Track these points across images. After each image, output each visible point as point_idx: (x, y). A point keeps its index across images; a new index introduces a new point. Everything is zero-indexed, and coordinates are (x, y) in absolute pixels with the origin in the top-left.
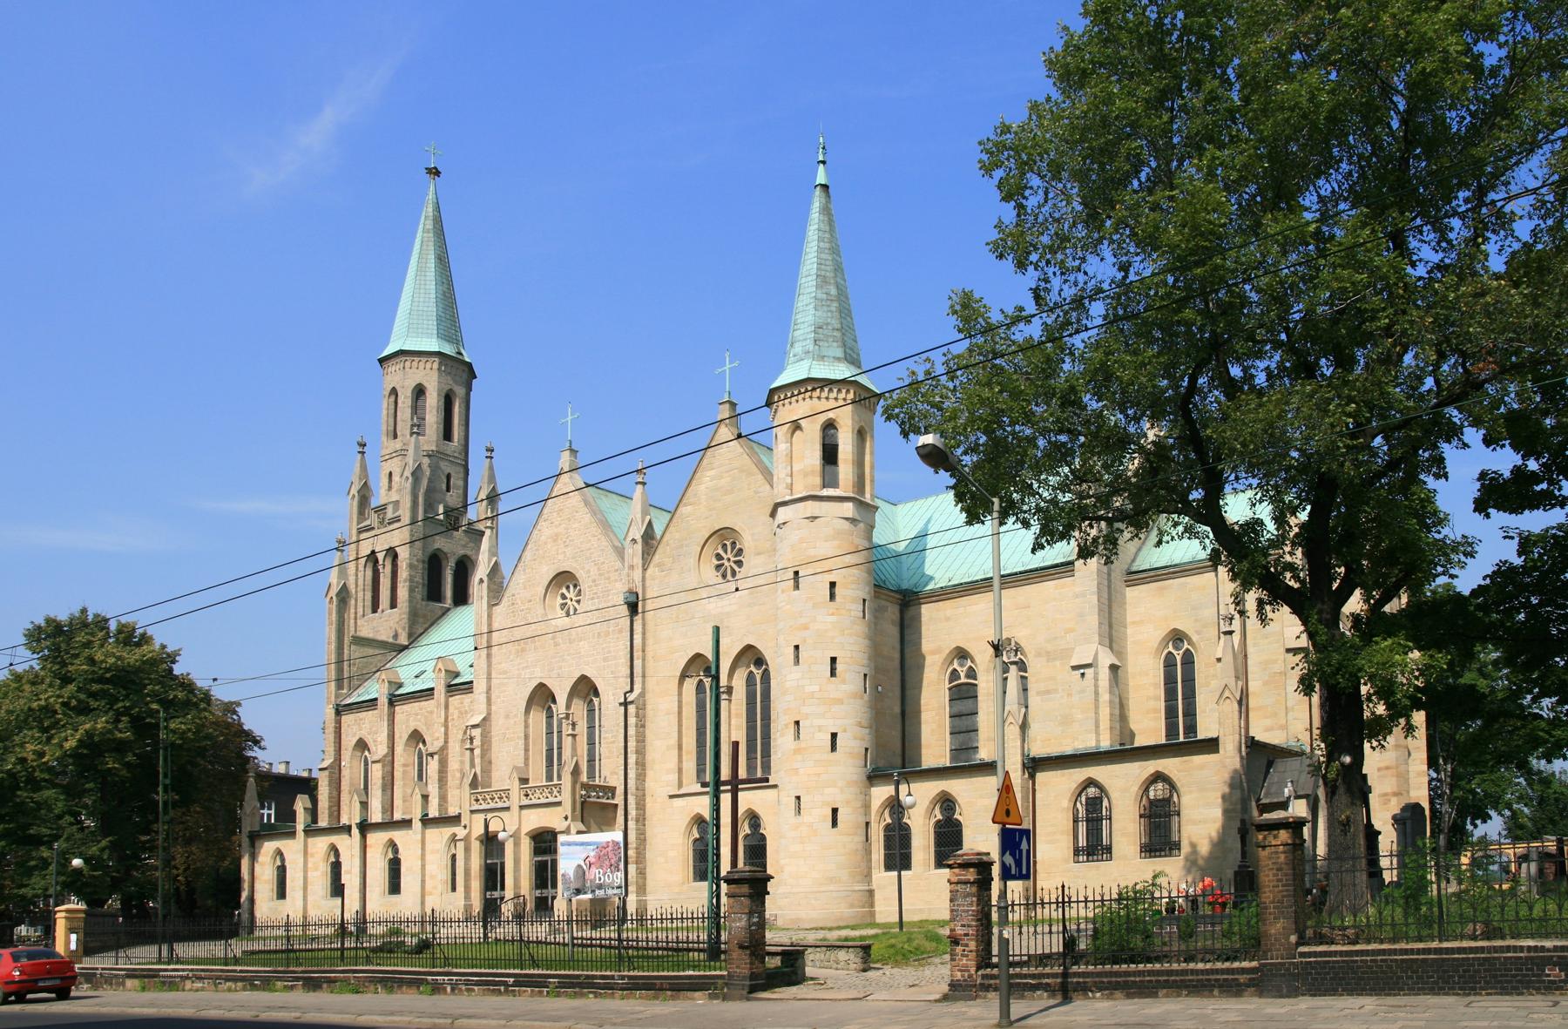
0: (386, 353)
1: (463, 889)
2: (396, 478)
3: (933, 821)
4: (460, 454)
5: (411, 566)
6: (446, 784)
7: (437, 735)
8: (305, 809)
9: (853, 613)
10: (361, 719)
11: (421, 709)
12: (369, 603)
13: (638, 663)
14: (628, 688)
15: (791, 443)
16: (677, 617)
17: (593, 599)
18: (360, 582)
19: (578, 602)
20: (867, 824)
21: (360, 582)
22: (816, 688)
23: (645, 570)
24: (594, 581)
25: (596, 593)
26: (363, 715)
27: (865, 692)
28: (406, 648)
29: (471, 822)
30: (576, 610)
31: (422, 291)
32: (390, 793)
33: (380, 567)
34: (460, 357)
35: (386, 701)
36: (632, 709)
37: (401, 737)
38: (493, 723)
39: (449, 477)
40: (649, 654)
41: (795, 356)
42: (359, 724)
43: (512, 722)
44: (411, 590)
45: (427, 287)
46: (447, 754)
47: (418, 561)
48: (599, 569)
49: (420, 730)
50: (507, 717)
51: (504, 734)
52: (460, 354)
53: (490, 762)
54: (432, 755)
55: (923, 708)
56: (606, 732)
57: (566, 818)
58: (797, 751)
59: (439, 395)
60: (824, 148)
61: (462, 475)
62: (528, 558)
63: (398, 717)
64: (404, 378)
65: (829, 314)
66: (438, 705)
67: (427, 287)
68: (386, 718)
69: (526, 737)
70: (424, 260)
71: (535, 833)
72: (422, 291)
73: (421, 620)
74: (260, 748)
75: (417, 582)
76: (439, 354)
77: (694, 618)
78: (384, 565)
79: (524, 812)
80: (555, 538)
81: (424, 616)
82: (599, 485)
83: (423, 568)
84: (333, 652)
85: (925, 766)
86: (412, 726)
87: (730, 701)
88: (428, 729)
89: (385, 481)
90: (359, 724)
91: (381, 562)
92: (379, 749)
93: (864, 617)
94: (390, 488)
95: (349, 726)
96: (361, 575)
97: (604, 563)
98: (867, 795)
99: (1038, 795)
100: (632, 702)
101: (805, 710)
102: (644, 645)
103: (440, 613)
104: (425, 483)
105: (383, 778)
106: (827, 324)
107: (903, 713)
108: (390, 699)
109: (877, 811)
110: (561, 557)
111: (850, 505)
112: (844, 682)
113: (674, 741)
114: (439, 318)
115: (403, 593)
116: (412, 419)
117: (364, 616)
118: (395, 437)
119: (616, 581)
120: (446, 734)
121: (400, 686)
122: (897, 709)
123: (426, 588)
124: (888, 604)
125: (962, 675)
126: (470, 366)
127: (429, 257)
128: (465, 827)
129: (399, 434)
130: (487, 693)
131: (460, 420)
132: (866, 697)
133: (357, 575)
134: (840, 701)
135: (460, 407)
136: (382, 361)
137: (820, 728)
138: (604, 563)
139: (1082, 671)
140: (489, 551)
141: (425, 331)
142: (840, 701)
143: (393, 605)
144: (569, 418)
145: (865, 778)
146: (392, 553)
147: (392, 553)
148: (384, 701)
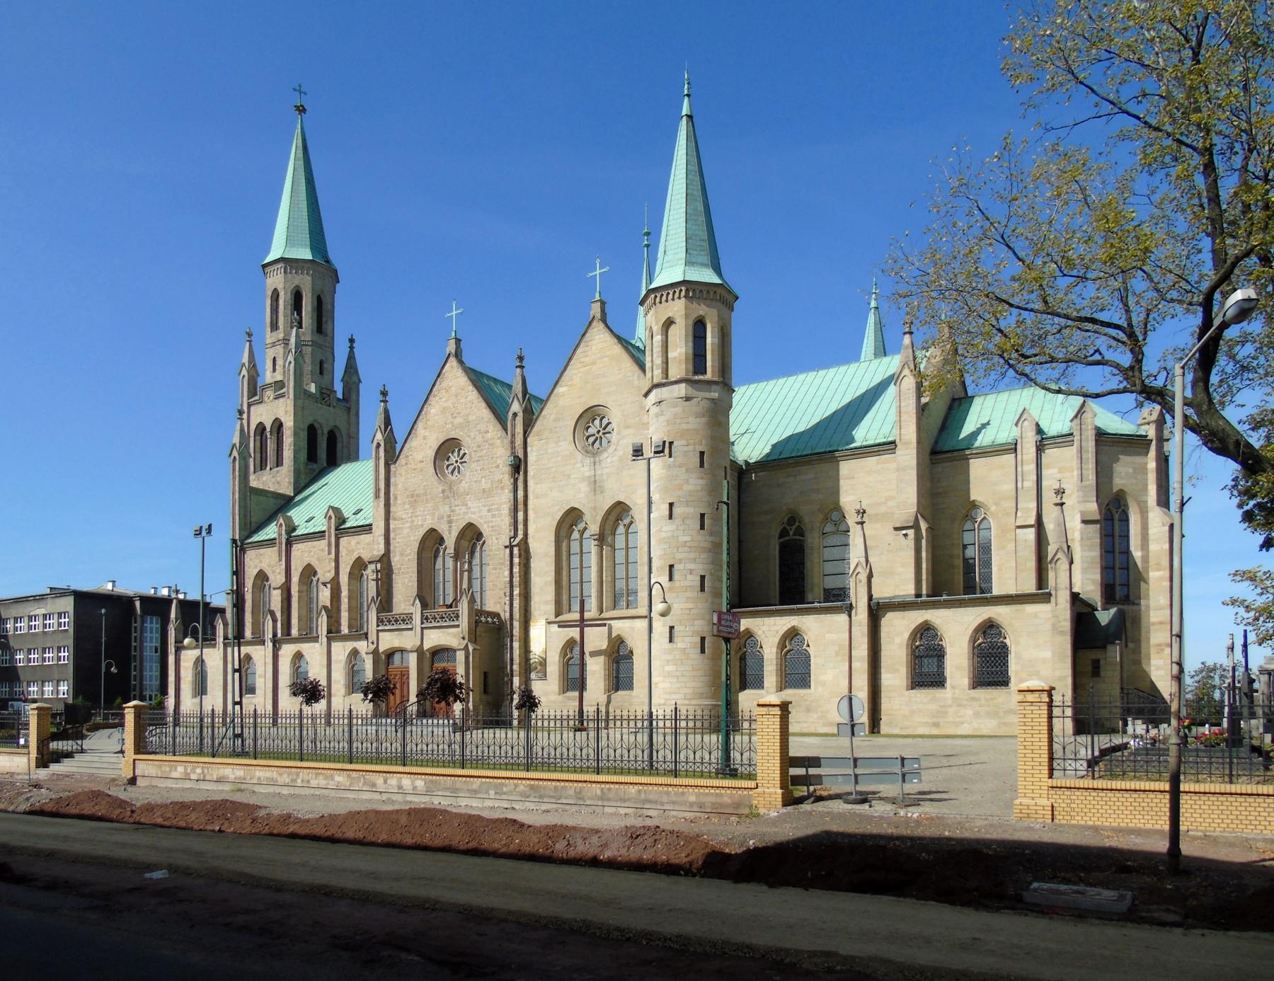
0: (268, 260)
2: (280, 362)
5: (296, 434)
10: (261, 555)
14: (512, 534)
17: (478, 461)
37: (296, 569)
43: (407, 559)
49: (312, 563)
60: (688, 83)
64: (276, 280)
65: (697, 227)
71: (434, 650)
85: (996, 592)
89: (269, 364)
92: (277, 578)
94: (274, 370)
102: (526, 497)
106: (696, 235)
111: (683, 385)
115: (288, 453)
125: (791, 533)
136: (264, 266)
139: (904, 532)
143: (279, 463)
144: (454, 313)
146: (278, 426)
147: (278, 426)
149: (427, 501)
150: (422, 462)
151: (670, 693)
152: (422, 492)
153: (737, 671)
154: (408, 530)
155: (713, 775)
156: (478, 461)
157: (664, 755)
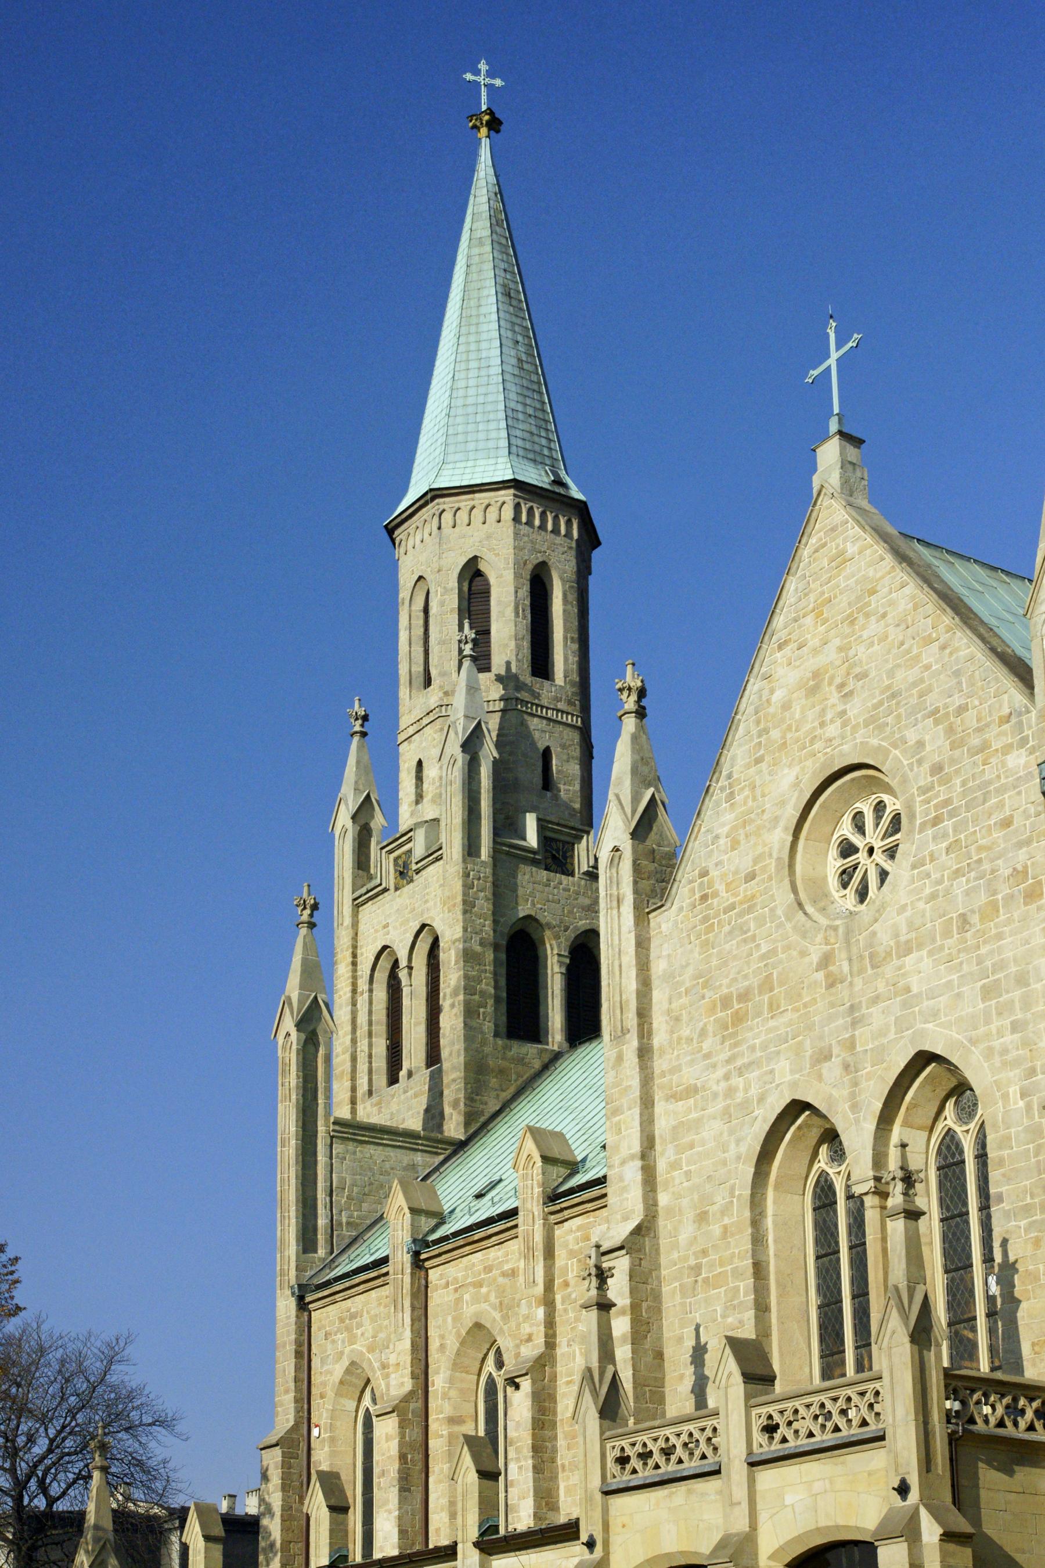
2: (431, 772)
4: (570, 703)
5: (468, 956)
6: (553, 1460)
7: (526, 1329)
8: (207, 1538)
10: (353, 1316)
11: (488, 1269)
12: (381, 1063)
17: (936, 821)
18: (362, 1019)
19: (891, 853)
21: (362, 1019)
24: (937, 769)
25: (947, 802)
26: (357, 1303)
28: (460, 1146)
29: (606, 1527)
30: (883, 875)
31: (473, 364)
32: (419, 1497)
33: (403, 975)
34: (562, 491)
35: (407, 1258)
38: (664, 1242)
39: (547, 754)
42: (348, 1329)
43: (716, 1229)
44: (470, 1012)
46: (554, 1378)
47: (482, 944)
48: (950, 730)
50: (702, 1218)
51: (697, 1269)
52: (558, 482)
53: (660, 1355)
54: (513, 1383)
56: (1007, 1215)
57: (903, 1490)
59: (517, 576)
61: (576, 752)
63: (437, 1299)
66: (528, 1253)
67: (484, 354)
68: (407, 1303)
69: (759, 1270)
70: (473, 303)
72: (473, 364)
73: (494, 1082)
74: (178, 1436)
75: (482, 993)
76: (516, 484)
78: (410, 968)
79: (767, 1477)
80: (813, 686)
81: (502, 1072)
83: (496, 960)
84: (293, 1161)
86: (470, 1312)
88: (506, 1318)
90: (348, 1329)
91: (403, 963)
94: (419, 798)
95: (327, 1336)
96: (362, 1001)
97: (962, 709)
103: (537, 1065)
104: (489, 752)
105: (403, 1457)
108: (417, 1254)
110: (832, 730)
114: (511, 417)
116: (461, 628)
117: (370, 1093)
118: (428, 682)
119: (1007, 749)
120: (550, 1323)
121: (441, 1220)
123: (503, 1008)
126: (581, 510)
127: (485, 292)
128: (590, 1545)
129: (434, 672)
130: (643, 1156)
131: (566, 630)
133: (354, 1004)
138: (962, 709)
140: (635, 771)
141: (481, 445)
148: (402, 1260)
149: (773, 1006)
150: (751, 877)
151: (693, 1053)
152: (755, 981)
153: (590, 1205)
154: (717, 1125)
155: (658, 887)
156: (936, 821)
157: (472, 596)
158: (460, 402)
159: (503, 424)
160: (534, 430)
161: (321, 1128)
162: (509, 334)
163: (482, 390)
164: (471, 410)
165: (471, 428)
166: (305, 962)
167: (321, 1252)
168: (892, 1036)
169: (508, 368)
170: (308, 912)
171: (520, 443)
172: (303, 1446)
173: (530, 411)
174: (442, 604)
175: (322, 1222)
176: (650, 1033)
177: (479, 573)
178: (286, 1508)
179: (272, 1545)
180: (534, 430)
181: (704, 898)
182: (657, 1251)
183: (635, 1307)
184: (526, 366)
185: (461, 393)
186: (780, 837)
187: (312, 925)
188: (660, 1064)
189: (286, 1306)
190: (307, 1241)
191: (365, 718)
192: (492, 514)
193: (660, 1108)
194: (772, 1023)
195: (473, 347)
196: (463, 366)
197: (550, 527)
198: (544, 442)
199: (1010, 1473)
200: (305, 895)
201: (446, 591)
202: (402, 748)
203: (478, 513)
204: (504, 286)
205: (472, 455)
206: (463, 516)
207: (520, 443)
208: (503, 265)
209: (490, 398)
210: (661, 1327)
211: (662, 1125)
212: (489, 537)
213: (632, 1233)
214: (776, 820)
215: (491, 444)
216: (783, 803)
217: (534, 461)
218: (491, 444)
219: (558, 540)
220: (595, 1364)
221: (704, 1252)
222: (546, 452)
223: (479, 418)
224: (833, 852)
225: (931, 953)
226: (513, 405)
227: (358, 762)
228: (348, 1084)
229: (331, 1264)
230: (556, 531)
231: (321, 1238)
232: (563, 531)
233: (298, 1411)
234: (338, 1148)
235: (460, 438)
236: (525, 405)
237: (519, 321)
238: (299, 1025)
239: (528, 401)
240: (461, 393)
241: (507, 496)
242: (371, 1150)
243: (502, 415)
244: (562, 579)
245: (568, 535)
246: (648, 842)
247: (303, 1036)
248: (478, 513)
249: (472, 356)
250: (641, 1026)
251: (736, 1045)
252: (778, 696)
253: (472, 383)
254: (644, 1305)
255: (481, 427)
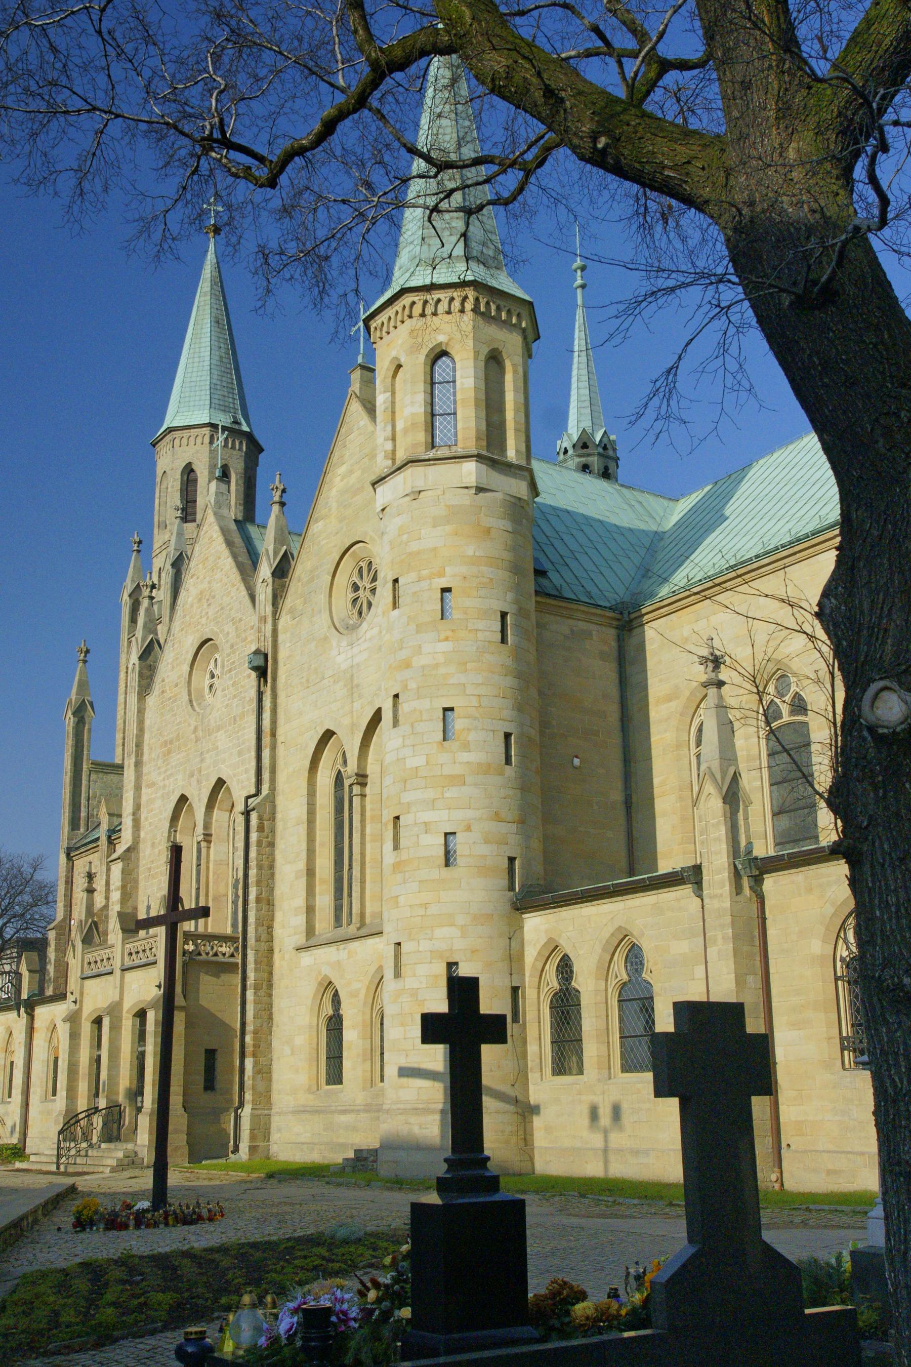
1: (64, 1093)
3: (612, 982)
9: (480, 635)
13: (266, 754)
14: (253, 791)
15: (393, 393)
16: (308, 681)
20: (515, 990)
22: (420, 761)
23: (275, 620)
27: (508, 761)
31: (197, 360)
34: (236, 427)
36: (254, 816)
40: (280, 738)
41: (400, 269)
45: (202, 354)
50: (153, 845)
52: (236, 422)
55: (656, 791)
58: (397, 867)
62: (177, 629)
67: (202, 354)
70: (199, 327)
72: (197, 360)
77: (323, 678)
82: (799, 629)
87: (363, 796)
93: (504, 640)
98: (514, 934)
99: (771, 932)
100: (253, 809)
101: (407, 797)
107: (628, 804)
109: (534, 966)
112: (466, 747)
113: (302, 865)
114: (213, 388)
122: (617, 796)
124: (592, 627)
127: (205, 321)
130: (134, 814)
132: (509, 771)
134: (458, 780)
135: (237, 484)
137: (427, 827)
138: (241, 620)
141: (197, 403)
142: (458, 780)
145: (508, 907)
148: (103, 841)
158: (188, 380)
159: (208, 392)
160: (226, 394)
161: (85, 767)
162: (216, 343)
163: (199, 374)
164: (193, 384)
165: (192, 394)
166: (80, 680)
167: (82, 830)
168: (212, 769)
169: (214, 362)
170: (83, 655)
171: (217, 401)
172: (67, 929)
173: (224, 384)
174: (173, 487)
175: (83, 814)
176: (142, 755)
177: (192, 471)
178: (57, 960)
179: (50, 979)
180: (226, 394)
181: (163, 692)
182: (138, 859)
183: (123, 887)
184: (224, 360)
185: (189, 375)
186: (186, 668)
187: (85, 662)
188: (145, 769)
189: (63, 858)
190: (74, 824)
191: (140, 542)
192: (199, 440)
193: (144, 790)
194: (178, 756)
195: (197, 350)
196: (191, 361)
197: (230, 446)
198: (231, 400)
199: (218, 976)
200: (82, 646)
201: (175, 480)
202: (155, 560)
203: (192, 440)
204: (215, 317)
205: (192, 409)
206: (184, 441)
207: (217, 401)
208: (216, 306)
209: (203, 378)
210: (137, 896)
211: (144, 799)
212: (197, 452)
213: (125, 851)
214: (185, 659)
215: (202, 403)
216: (187, 652)
217: (224, 411)
218: (202, 403)
219: (235, 452)
220: (83, 918)
221: (152, 862)
222: (231, 405)
223: (197, 388)
224: (208, 676)
225: (225, 732)
226: (214, 381)
227: (134, 566)
228: (122, 735)
229: (85, 837)
230: (233, 447)
231: (82, 823)
232: (237, 447)
233: (65, 911)
234: (93, 776)
235: (187, 399)
236: (222, 381)
237: (222, 336)
238: (74, 714)
239: (224, 379)
240: (189, 375)
241: (207, 431)
242: (112, 776)
243: (208, 387)
244: (236, 474)
245: (240, 449)
246: (148, 662)
247: (76, 719)
248: (192, 440)
249: (196, 355)
250: (137, 752)
251: (168, 764)
252: (190, 599)
253: (195, 370)
254: (129, 885)
255: (198, 393)
